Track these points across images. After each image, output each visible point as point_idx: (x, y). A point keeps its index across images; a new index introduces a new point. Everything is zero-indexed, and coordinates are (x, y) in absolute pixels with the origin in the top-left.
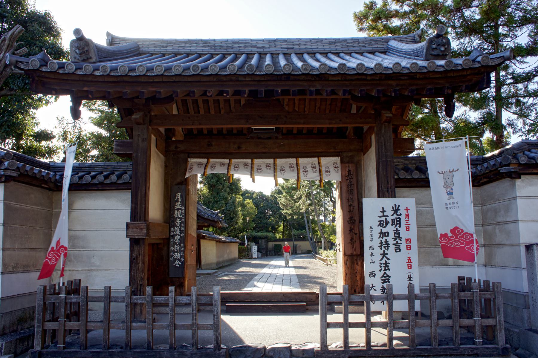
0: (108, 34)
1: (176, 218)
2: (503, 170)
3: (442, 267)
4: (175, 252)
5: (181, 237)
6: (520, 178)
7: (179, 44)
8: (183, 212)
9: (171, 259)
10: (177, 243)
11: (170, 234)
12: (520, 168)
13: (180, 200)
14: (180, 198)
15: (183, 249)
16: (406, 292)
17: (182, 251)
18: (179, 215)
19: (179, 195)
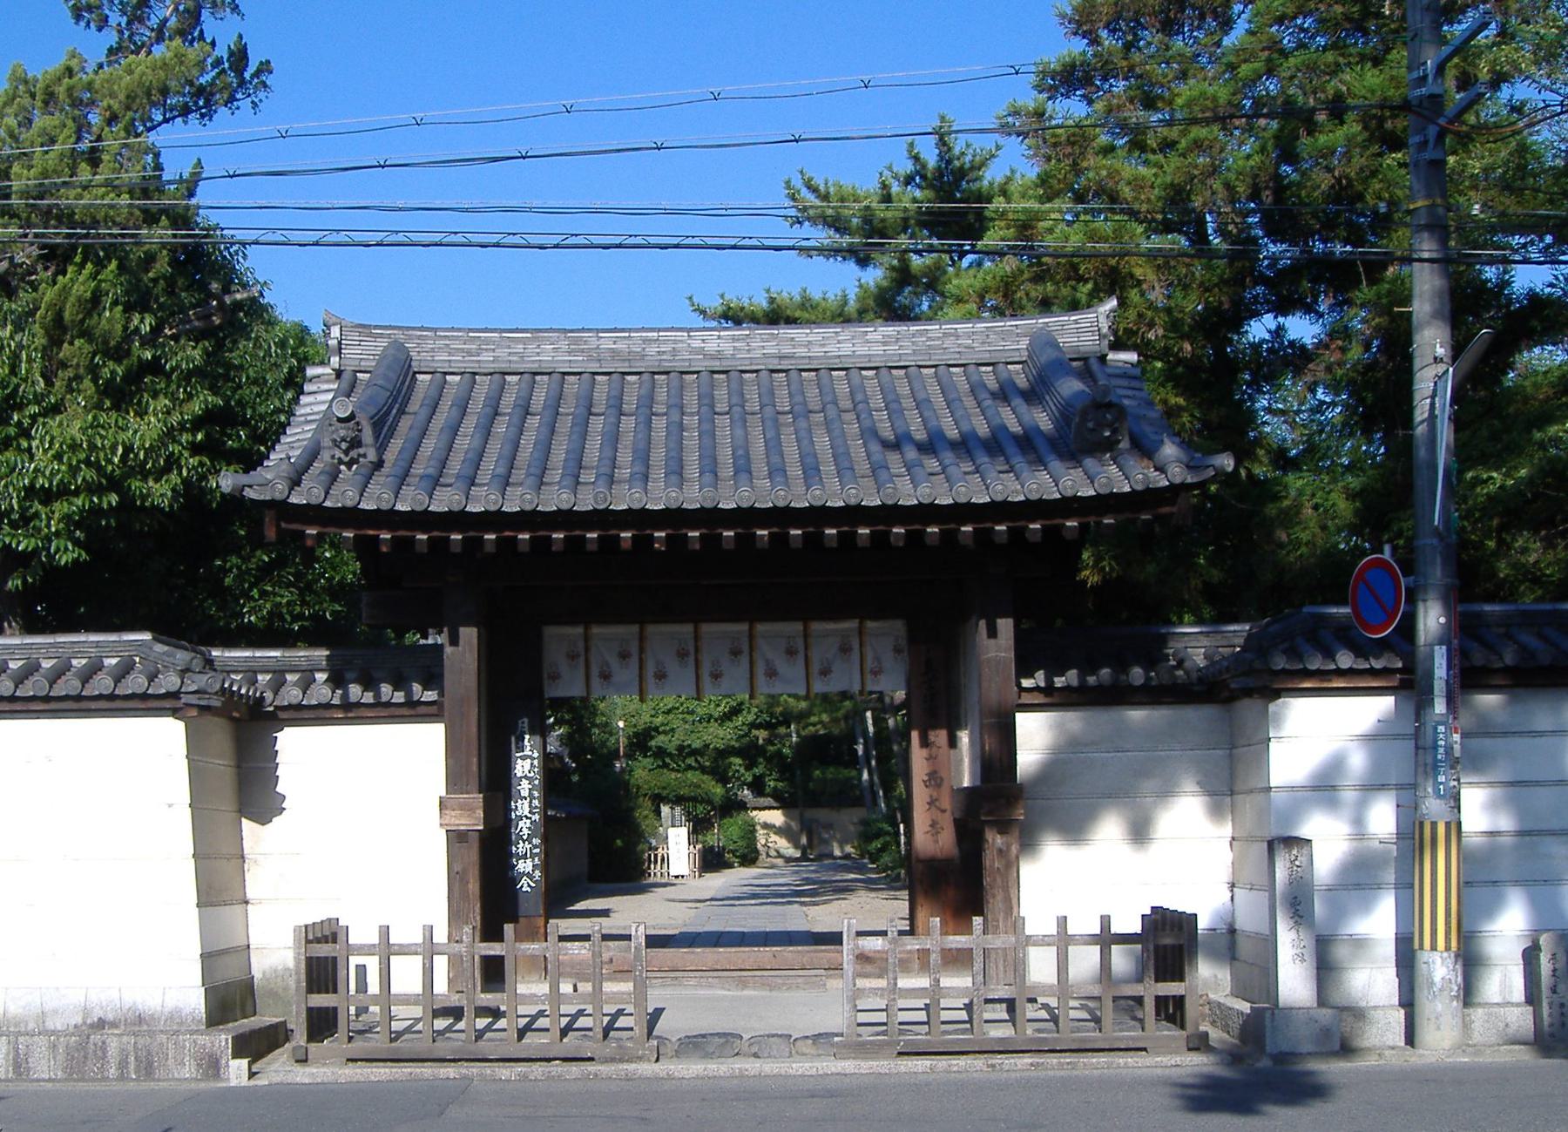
7: (509, 347)
16: (1052, 929)
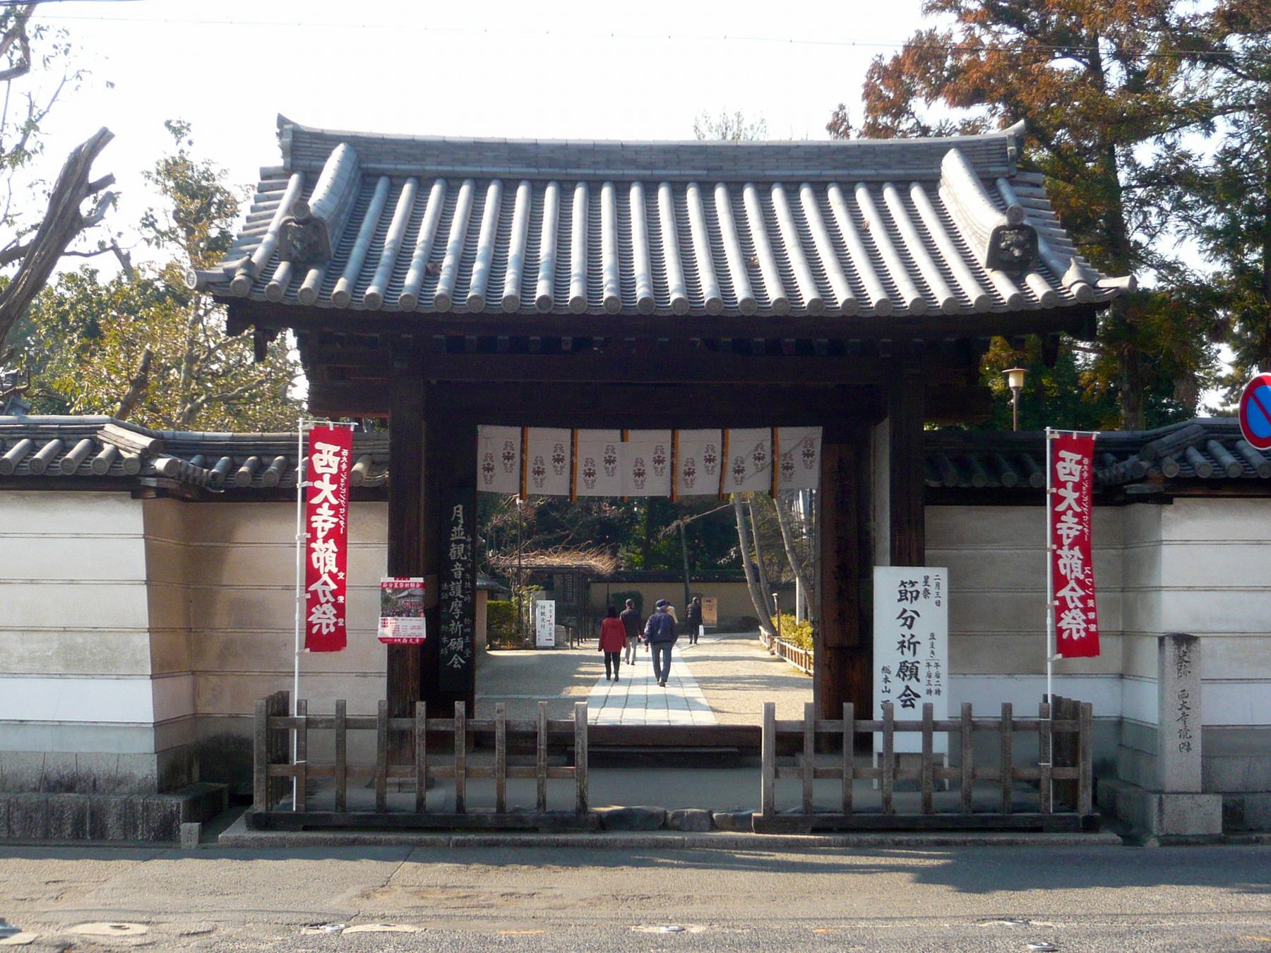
0: (282, 121)
1: (454, 562)
2: (1132, 489)
3: (1025, 676)
4: (450, 636)
5: (464, 603)
6: (1171, 503)
8: (469, 547)
9: (444, 651)
10: (457, 617)
11: (439, 596)
12: (1167, 485)
13: (461, 522)
14: (461, 515)
15: (468, 630)
17: (467, 634)
18: (459, 553)
19: (459, 510)
